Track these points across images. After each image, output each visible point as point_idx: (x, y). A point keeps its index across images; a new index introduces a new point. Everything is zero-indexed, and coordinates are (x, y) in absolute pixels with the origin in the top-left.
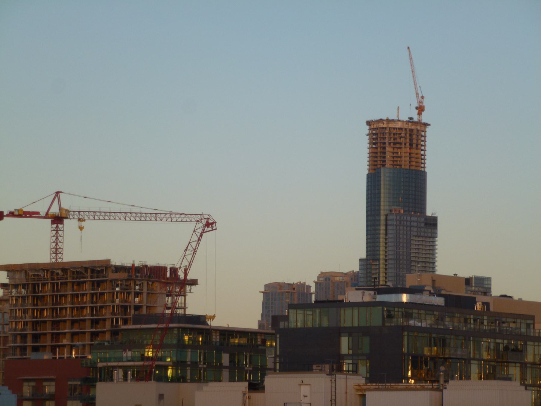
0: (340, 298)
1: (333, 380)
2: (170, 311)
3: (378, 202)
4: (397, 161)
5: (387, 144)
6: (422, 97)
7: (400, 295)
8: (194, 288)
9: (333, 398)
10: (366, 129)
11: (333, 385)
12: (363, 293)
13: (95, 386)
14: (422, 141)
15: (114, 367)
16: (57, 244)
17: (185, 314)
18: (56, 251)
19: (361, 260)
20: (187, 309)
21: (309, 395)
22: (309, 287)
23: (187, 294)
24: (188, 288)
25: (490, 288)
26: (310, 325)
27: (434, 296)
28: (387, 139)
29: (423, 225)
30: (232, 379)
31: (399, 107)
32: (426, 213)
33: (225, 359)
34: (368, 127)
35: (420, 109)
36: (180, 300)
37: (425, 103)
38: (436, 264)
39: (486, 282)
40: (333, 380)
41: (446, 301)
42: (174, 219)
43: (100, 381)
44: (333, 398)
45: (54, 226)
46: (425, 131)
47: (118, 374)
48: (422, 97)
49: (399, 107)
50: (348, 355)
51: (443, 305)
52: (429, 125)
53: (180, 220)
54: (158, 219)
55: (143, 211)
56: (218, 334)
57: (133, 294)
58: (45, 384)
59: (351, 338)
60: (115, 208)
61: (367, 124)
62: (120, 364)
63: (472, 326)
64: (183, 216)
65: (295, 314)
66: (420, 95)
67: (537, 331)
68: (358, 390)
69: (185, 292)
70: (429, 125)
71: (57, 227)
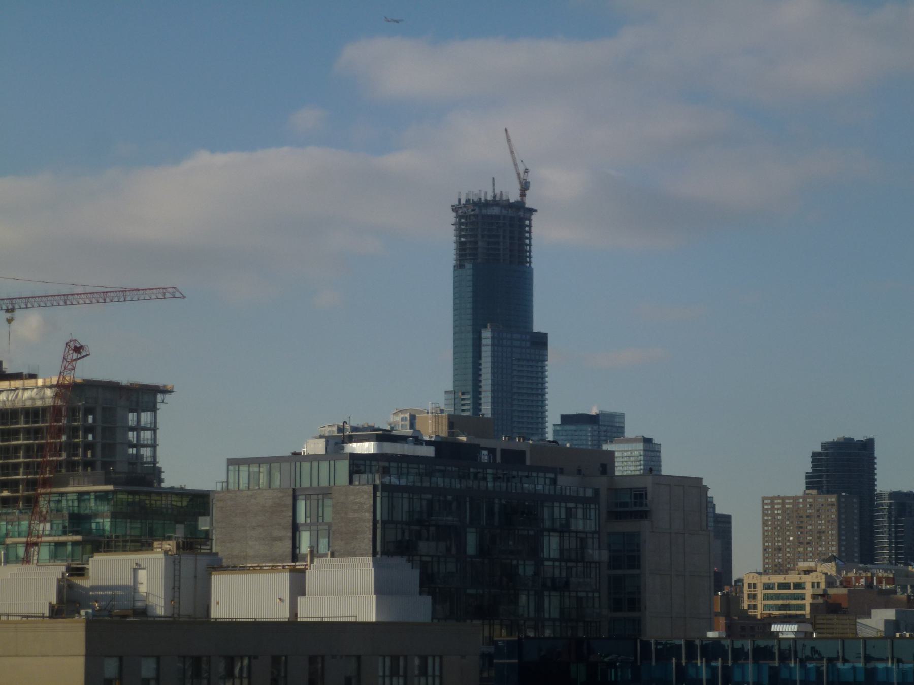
3: (464, 249)
4: (494, 247)
5: (480, 236)
6: (526, 171)
7: (382, 619)
8: (168, 397)
10: (452, 217)
12: (327, 442)
14: (527, 232)
19: (446, 392)
23: (159, 406)
25: (623, 427)
26: (547, 492)
27: (422, 444)
29: (528, 344)
32: (532, 328)
34: (454, 214)
35: (525, 187)
36: (146, 417)
37: (530, 178)
38: (547, 396)
39: (617, 420)
41: (436, 451)
42: (129, 298)
46: (530, 220)
48: (526, 171)
50: (306, 524)
51: (323, 452)
52: (535, 211)
53: (136, 298)
54: (108, 300)
55: (88, 290)
59: (308, 502)
60: (53, 290)
61: (453, 210)
63: (490, 485)
64: (141, 292)
66: (521, 169)
67: (558, 487)
69: (155, 403)
70: (535, 211)
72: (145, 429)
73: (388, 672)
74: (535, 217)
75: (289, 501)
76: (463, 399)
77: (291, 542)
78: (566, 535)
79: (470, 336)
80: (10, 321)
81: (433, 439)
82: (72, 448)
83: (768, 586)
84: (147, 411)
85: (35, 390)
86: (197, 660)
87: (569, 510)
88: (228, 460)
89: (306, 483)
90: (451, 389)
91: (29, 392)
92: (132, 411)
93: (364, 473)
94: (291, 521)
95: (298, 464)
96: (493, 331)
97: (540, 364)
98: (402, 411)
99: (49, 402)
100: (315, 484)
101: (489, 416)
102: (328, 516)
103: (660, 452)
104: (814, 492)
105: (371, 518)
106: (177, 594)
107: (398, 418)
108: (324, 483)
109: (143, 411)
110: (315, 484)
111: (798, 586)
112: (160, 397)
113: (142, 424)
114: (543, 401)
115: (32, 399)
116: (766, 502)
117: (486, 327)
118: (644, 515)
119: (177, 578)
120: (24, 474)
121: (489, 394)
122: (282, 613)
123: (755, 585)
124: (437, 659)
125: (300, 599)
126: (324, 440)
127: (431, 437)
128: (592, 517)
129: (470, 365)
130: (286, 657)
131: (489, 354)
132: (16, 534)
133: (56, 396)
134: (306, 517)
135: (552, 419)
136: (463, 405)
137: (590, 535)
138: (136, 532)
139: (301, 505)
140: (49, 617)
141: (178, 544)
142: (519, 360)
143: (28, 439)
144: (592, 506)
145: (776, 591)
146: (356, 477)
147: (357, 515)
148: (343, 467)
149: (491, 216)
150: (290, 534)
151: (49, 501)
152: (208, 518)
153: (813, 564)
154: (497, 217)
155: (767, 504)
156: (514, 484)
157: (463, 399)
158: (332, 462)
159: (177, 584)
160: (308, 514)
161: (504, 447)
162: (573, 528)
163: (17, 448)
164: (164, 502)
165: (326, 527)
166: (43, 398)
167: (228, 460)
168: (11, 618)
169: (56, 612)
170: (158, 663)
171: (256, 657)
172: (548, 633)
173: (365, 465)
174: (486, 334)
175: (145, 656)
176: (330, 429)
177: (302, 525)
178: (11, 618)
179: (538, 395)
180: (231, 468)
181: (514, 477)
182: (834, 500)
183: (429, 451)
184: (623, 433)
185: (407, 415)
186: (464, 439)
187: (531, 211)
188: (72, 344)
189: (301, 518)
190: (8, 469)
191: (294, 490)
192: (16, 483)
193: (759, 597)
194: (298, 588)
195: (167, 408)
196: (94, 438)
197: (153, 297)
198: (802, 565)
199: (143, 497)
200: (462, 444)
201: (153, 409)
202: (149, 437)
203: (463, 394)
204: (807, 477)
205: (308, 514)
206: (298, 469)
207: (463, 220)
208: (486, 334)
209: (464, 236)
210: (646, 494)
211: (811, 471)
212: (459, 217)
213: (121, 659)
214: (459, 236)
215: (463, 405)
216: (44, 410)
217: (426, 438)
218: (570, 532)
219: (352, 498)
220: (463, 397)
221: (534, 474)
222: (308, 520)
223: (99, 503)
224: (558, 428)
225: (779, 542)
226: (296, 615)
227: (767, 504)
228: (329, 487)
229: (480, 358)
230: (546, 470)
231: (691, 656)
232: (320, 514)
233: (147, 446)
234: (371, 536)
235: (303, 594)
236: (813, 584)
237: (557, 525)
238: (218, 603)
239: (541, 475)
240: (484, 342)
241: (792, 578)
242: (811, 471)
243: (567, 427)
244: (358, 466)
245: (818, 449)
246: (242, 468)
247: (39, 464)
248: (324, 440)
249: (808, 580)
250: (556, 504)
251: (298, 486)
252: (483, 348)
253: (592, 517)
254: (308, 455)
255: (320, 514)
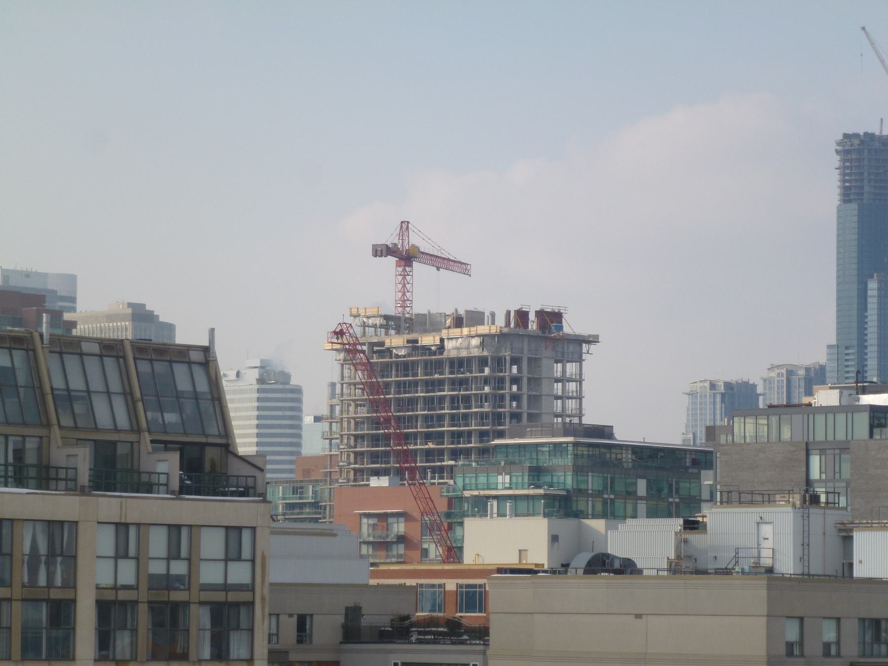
0: (806, 400)
1: (805, 516)
2: (560, 420)
3: (849, 195)
5: (866, 181)
8: (593, 348)
9: (806, 540)
11: (806, 522)
12: (841, 393)
13: (461, 524)
15: (488, 497)
16: (404, 294)
17: (580, 424)
18: (404, 302)
19: (829, 347)
20: (583, 418)
21: (771, 538)
22: (754, 386)
28: (866, 174)
30: (652, 513)
33: (642, 487)
40: (805, 516)
43: (299, 445)
44: (806, 540)
45: (400, 269)
47: (492, 506)
52: (592, 340)
56: (630, 452)
57: (508, 398)
58: (390, 520)
59: (823, 457)
62: (494, 493)
65: (742, 425)
68: (840, 530)
70: (592, 340)
71: (404, 270)
72: (570, 380)
76: (847, 354)
79: (855, 286)
84: (572, 362)
85: (460, 340)
86: (876, 623)
89: (820, 437)
90: (834, 342)
91: (454, 341)
92: (557, 362)
94: (804, 477)
95: (811, 417)
96: (880, 282)
98: (778, 367)
99: (476, 352)
106: (806, 552)
107: (773, 374)
108: (841, 436)
109: (568, 362)
113: (568, 375)
115: (458, 349)
117: (872, 277)
119: (806, 534)
120: (422, 427)
121: (875, 348)
129: (855, 319)
131: (875, 306)
132: (473, 487)
133: (482, 345)
134: (821, 473)
136: (847, 360)
143: (453, 390)
146: (876, 430)
148: (862, 421)
152: (710, 473)
157: (847, 354)
158: (850, 415)
163: (441, 399)
164: (624, 456)
165: (844, 484)
166: (468, 348)
169: (674, 569)
174: (873, 286)
176: (701, 384)
177: (817, 481)
185: (784, 371)
189: (815, 474)
190: (432, 421)
191: (807, 443)
192: (441, 435)
195: (593, 357)
196: (518, 389)
199: (603, 450)
201: (580, 360)
202: (574, 389)
203: (847, 348)
205: (823, 470)
207: (848, 164)
208: (873, 286)
209: (849, 181)
212: (844, 161)
214: (844, 181)
215: (847, 360)
216: (469, 360)
220: (847, 352)
222: (824, 476)
228: (847, 441)
232: (837, 470)
233: (572, 398)
238: (861, 562)
240: (870, 293)
244: (879, 419)
247: (410, 417)
251: (811, 439)
252: (869, 300)
254: (821, 407)
255: (837, 470)
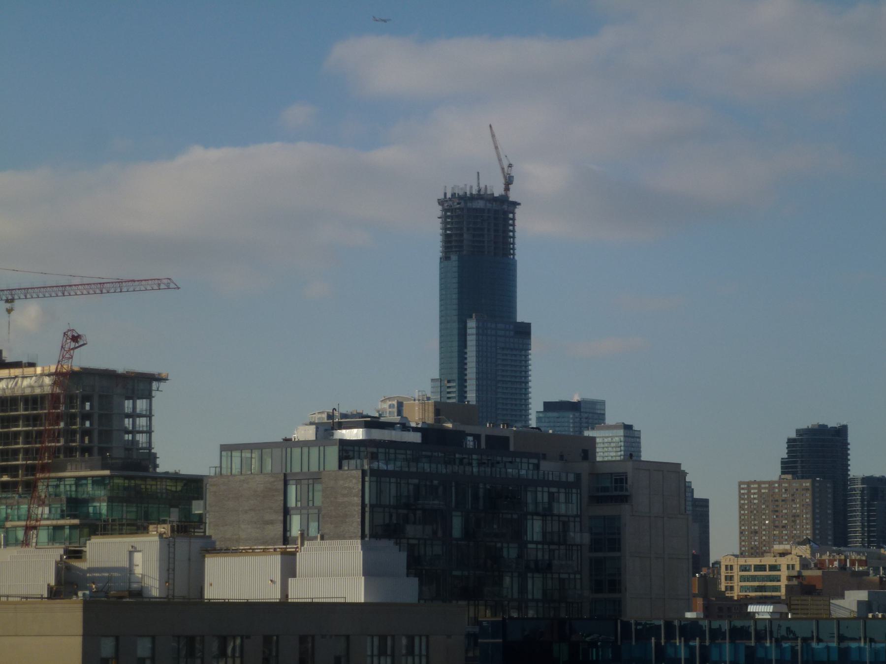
3: (450, 242)
4: (479, 239)
5: (465, 229)
6: (510, 166)
8: (162, 385)
10: (438, 211)
12: (317, 428)
14: (511, 225)
19: (432, 380)
23: (154, 393)
24: (155, 385)
25: (604, 414)
27: (409, 431)
29: (512, 333)
31: (490, 126)
32: (515, 318)
34: (440, 208)
35: (509, 182)
36: (141, 405)
37: (514, 172)
38: (530, 384)
39: (598, 407)
41: (423, 437)
42: (125, 289)
46: (514, 213)
48: (510, 166)
49: (490, 126)
50: (296, 508)
51: (313, 438)
52: (519, 204)
53: (131, 289)
54: (104, 291)
59: (299, 487)
61: (439, 203)
63: (475, 470)
64: (137, 283)
66: (505, 164)
67: (541, 472)
69: (150, 391)
70: (519, 204)
72: (140, 416)
73: (376, 652)
74: (518, 211)
75: (281, 485)
76: (449, 387)
77: (282, 525)
78: (549, 518)
79: (455, 325)
80: (9, 311)
81: (420, 426)
82: (70, 434)
83: (744, 568)
84: (143, 398)
85: (34, 378)
86: (191, 640)
87: (551, 495)
88: (221, 446)
89: (296, 469)
90: (438, 377)
91: (28, 380)
92: (128, 398)
93: (353, 458)
94: (282, 505)
95: (289, 450)
96: (478, 321)
97: (523, 353)
98: (390, 399)
99: (47, 390)
100: (305, 469)
101: (474, 403)
102: (318, 500)
103: (639, 438)
104: (789, 477)
105: (360, 502)
106: (171, 576)
107: (386, 406)
108: (314, 468)
109: (139, 398)
110: (305, 469)
111: (774, 568)
112: (155, 385)
113: (138, 411)
114: (527, 389)
115: (31, 387)
116: (742, 486)
117: (471, 317)
118: (624, 499)
119: (171, 560)
120: (23, 460)
121: (474, 382)
122: (273, 594)
123: (731, 567)
124: (424, 639)
125: (291, 581)
126: (314, 427)
127: (417, 424)
128: (574, 501)
129: (456, 354)
130: (277, 637)
131: (474, 343)
132: (16, 517)
133: (55, 383)
134: (296, 501)
135: (536, 406)
136: (449, 393)
137: (572, 519)
138: (132, 516)
139: (292, 489)
140: (48, 598)
141: (172, 527)
142: (503, 349)
143: (28, 426)
144: (574, 491)
145: (752, 573)
146: (345, 462)
147: (346, 499)
148: (333, 453)
149: (476, 210)
150: (281, 518)
151: (48, 486)
152: (201, 502)
153: (788, 547)
154: (481, 210)
155: (743, 489)
156: (498, 469)
157: (449, 387)
158: (322, 448)
159: (171, 566)
160: (299, 498)
161: (488, 433)
162: (555, 512)
163: (16, 435)
164: (159, 487)
165: (316, 511)
166: (41, 386)
167: (221, 446)
168: (10, 599)
169: (54, 593)
170: (153, 643)
171: (248, 637)
172: (531, 613)
173: (354, 451)
174: (472, 324)
175: (141, 636)
176: (320, 416)
177: (293, 508)
178: (10, 599)
179: (521, 383)
180: (224, 453)
181: (498, 463)
182: (808, 484)
183: (416, 438)
184: (604, 419)
185: (395, 403)
186: (449, 425)
187: (515, 204)
188: (70, 334)
189: (292, 503)
190: (7, 455)
191: (285, 475)
192: (16, 468)
193: (736, 578)
194: (289, 570)
195: (161, 396)
196: (91, 424)
197: (149, 288)
198: (778, 547)
199: (138, 482)
200: (448, 431)
201: (149, 396)
202: (145, 424)
203: (449, 382)
204: (782, 463)
205: (299, 498)
206: (289, 455)
207: (449, 214)
208: (472, 324)
209: (450, 229)
210: (626, 479)
211: (786, 456)
212: (445, 210)
213: (117, 639)
214: (445, 229)
215: (449, 393)
216: (43, 397)
217: (413, 425)
218: (552, 515)
219: (341, 482)
220: (449, 385)
221: (518, 460)
222: (299, 504)
223: (96, 487)
224: (541, 415)
225: (755, 525)
226: (287, 596)
227: (743, 489)
228: (319, 472)
229: (465, 347)
230: (530, 455)
231: (670, 635)
232: (311, 498)
233: (142, 432)
234: (359, 520)
235: (294, 576)
236: (788, 566)
237: (540, 509)
238: (211, 585)
239: (525, 460)
240: (469, 331)
241: (768, 560)
242: (786, 456)
243: (550, 414)
244: (347, 451)
245: (793, 435)
246: (234, 454)
247: (38, 449)
248: (314, 427)
249: (783, 562)
250: (539, 489)
251: (289, 471)
252: (469, 338)
253: (574, 501)
254: (299, 442)
255: (311, 498)
